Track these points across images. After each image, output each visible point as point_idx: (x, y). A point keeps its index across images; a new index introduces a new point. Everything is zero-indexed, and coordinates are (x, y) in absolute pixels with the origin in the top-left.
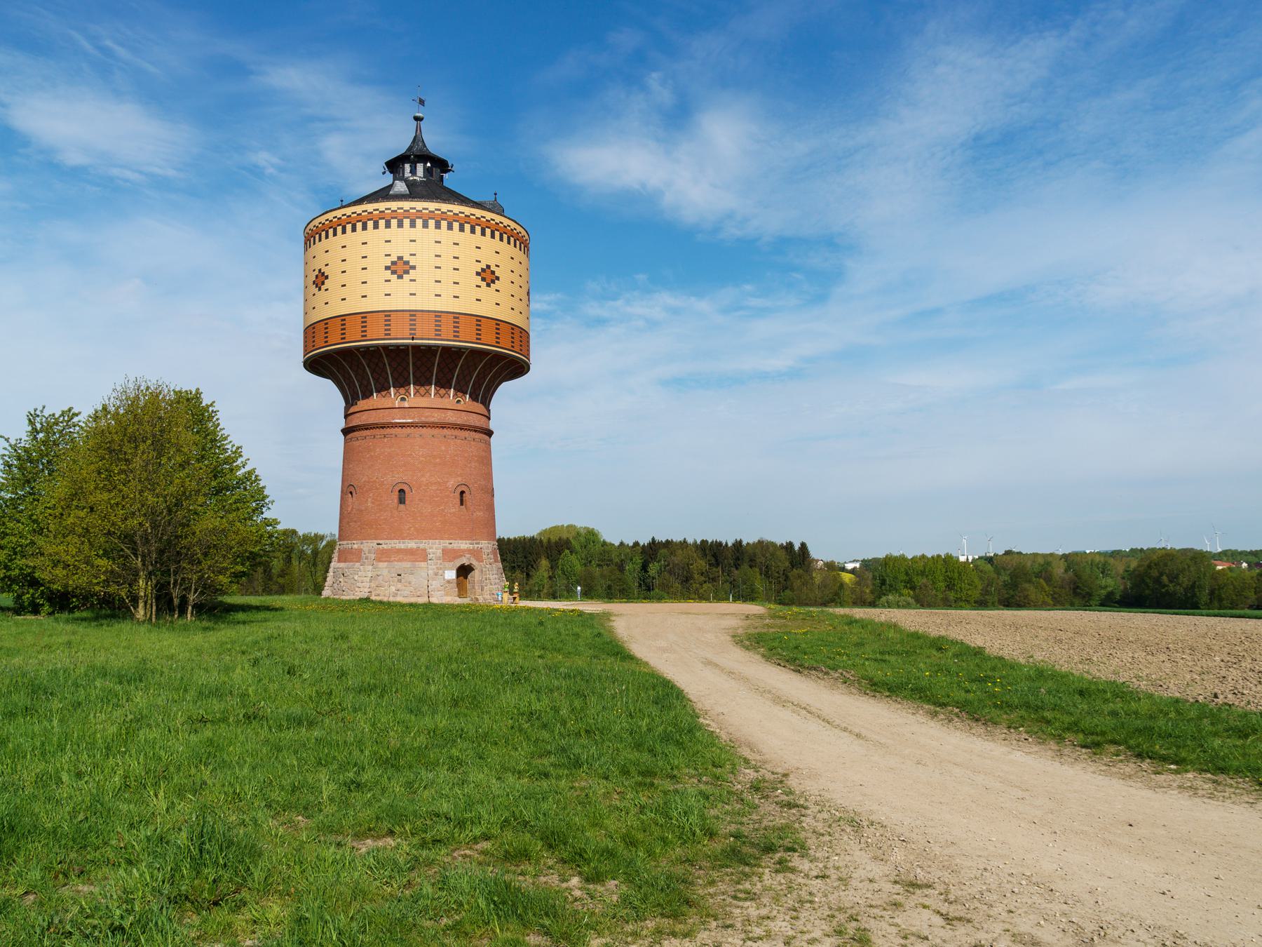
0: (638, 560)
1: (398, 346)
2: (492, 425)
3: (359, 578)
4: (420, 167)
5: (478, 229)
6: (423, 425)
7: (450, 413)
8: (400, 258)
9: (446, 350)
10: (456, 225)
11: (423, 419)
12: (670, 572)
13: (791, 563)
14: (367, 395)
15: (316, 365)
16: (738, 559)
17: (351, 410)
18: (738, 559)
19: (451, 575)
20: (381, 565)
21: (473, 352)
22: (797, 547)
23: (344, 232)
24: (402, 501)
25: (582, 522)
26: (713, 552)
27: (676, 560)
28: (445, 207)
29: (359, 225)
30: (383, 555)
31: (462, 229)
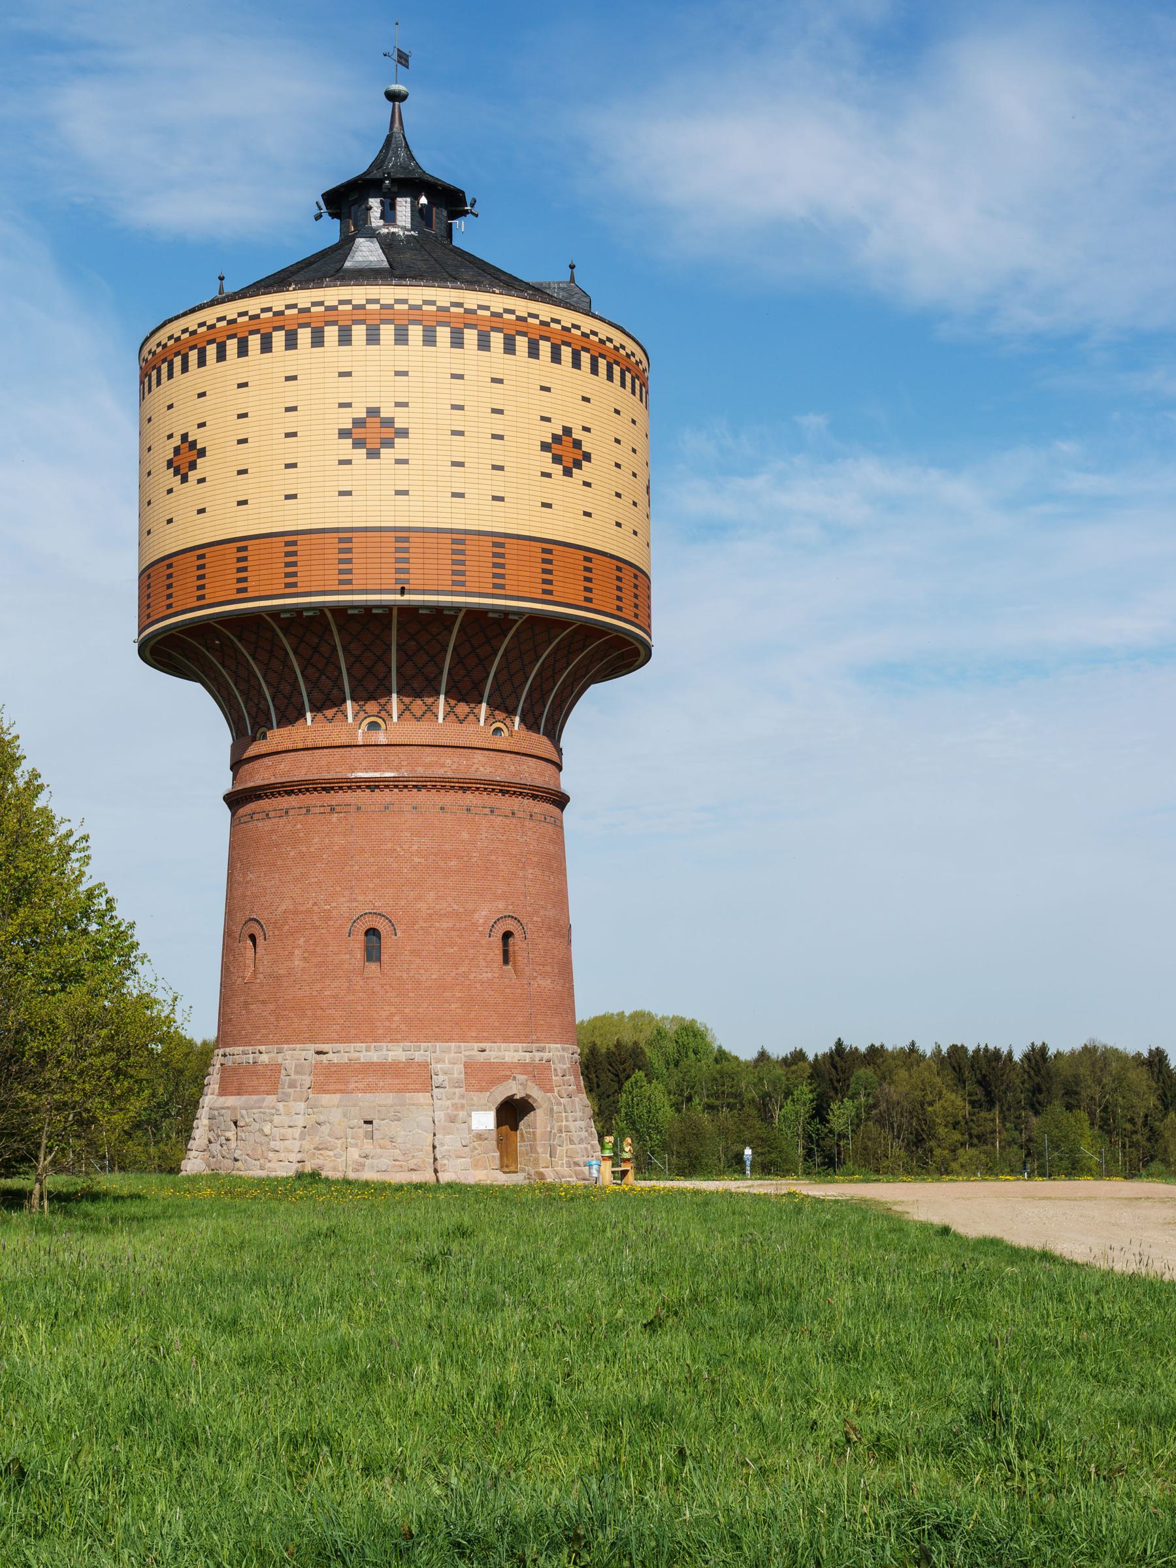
0: (805, 1093)
1: (367, 609)
2: (567, 783)
3: (276, 1127)
4: (404, 207)
5: (522, 343)
7: (479, 756)
8: (373, 412)
9: (476, 615)
10: (497, 339)
11: (420, 771)
12: (880, 1121)
13: (1162, 1098)
14: (291, 715)
15: (166, 651)
16: (1038, 1089)
17: (252, 751)
18: (1038, 1089)
19: (485, 1120)
20: (325, 1099)
21: (536, 621)
23: (243, 351)
24: (373, 953)
26: (981, 1076)
27: (894, 1092)
28: (472, 299)
29: (254, 342)
30: (331, 1079)
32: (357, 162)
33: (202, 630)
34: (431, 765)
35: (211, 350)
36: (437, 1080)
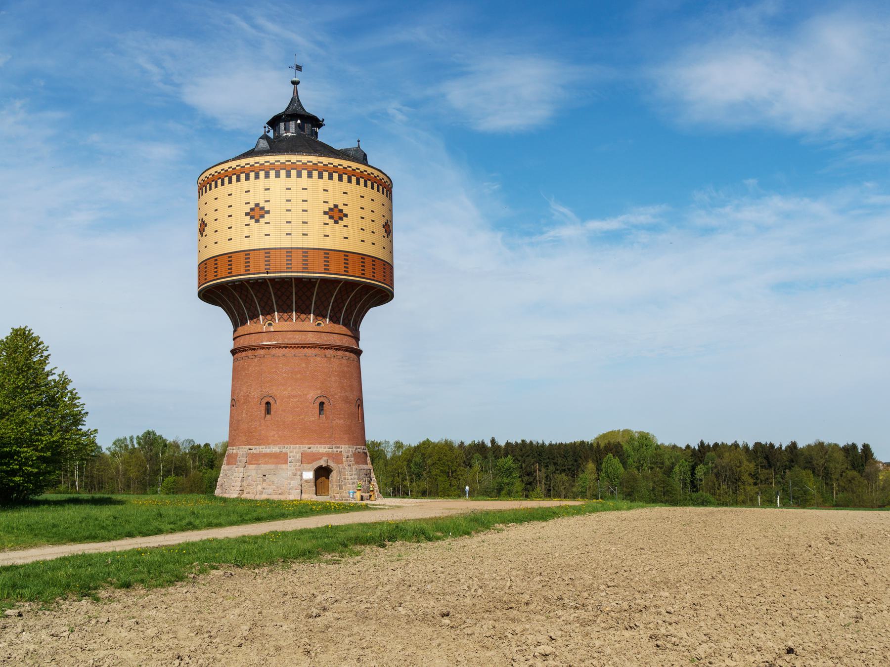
1: (256, 280)
5: (345, 177)
6: (286, 346)
7: (310, 334)
11: (286, 341)
15: (209, 295)
19: (309, 475)
21: (324, 281)
22: (860, 447)
23: (247, 178)
24: (268, 411)
25: (637, 427)
26: (765, 455)
29: (243, 176)
30: (253, 459)
31: (331, 177)
32: (281, 107)
33: (221, 287)
34: (290, 339)
35: (226, 179)
36: (290, 459)
